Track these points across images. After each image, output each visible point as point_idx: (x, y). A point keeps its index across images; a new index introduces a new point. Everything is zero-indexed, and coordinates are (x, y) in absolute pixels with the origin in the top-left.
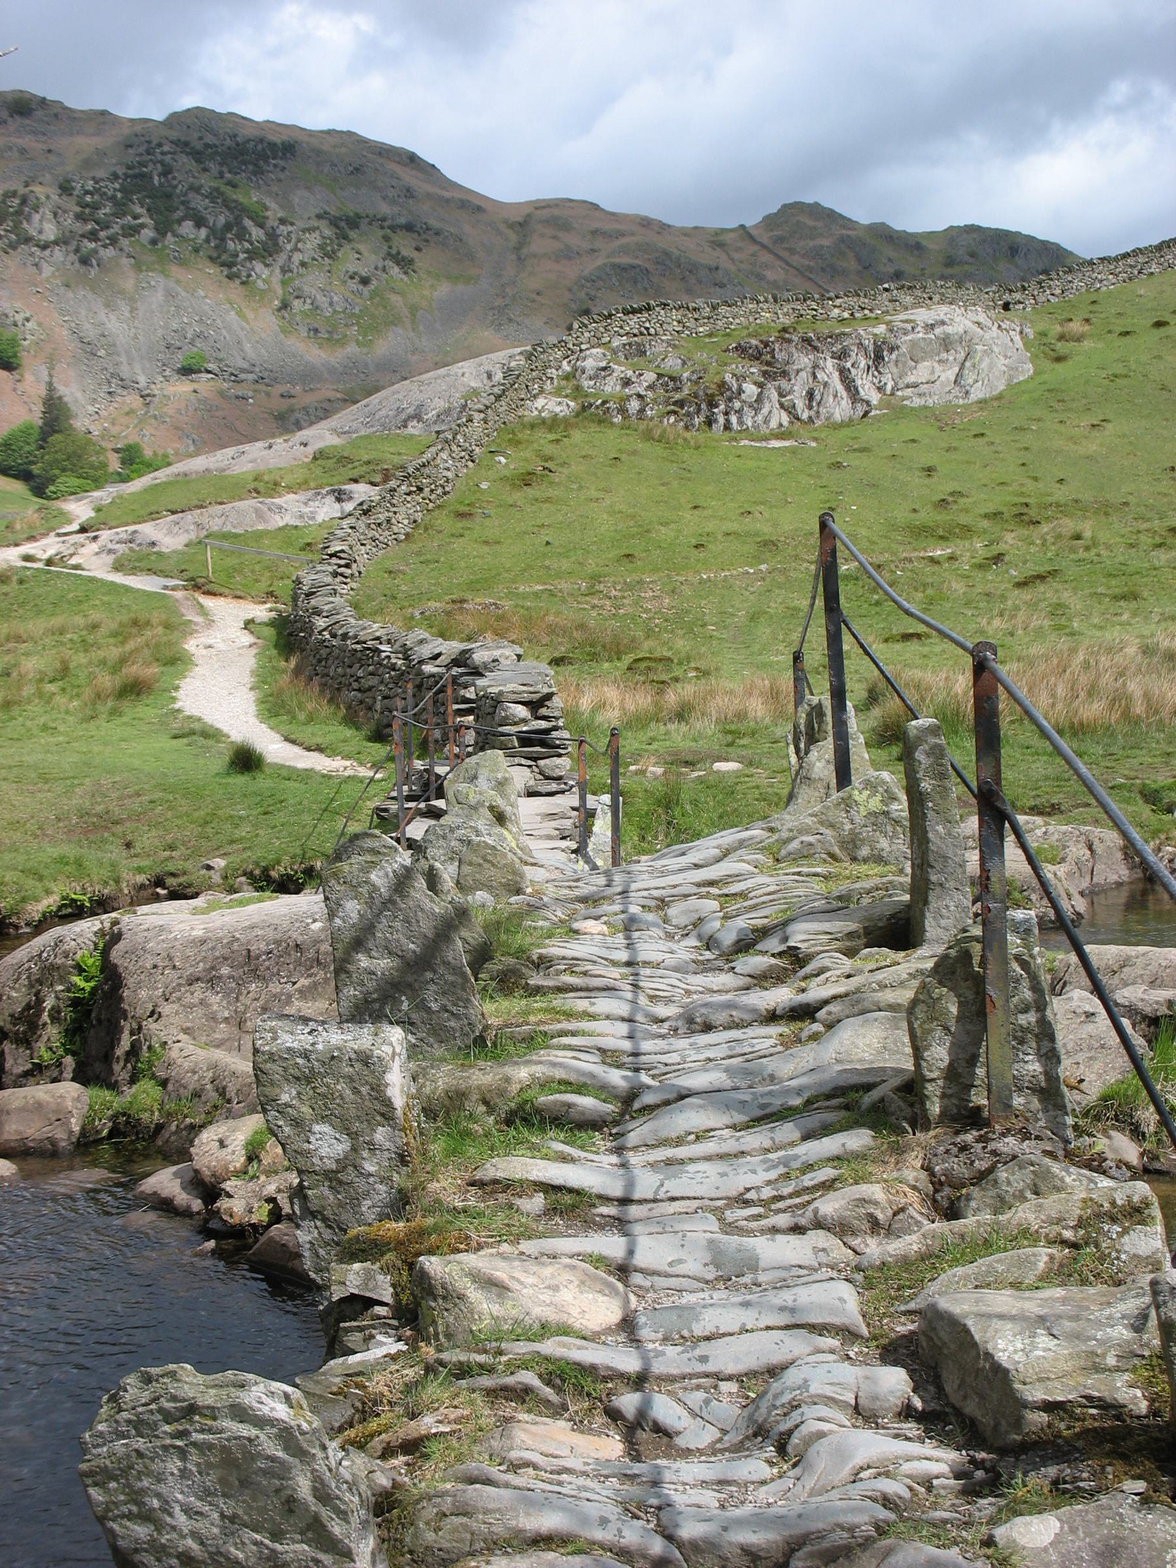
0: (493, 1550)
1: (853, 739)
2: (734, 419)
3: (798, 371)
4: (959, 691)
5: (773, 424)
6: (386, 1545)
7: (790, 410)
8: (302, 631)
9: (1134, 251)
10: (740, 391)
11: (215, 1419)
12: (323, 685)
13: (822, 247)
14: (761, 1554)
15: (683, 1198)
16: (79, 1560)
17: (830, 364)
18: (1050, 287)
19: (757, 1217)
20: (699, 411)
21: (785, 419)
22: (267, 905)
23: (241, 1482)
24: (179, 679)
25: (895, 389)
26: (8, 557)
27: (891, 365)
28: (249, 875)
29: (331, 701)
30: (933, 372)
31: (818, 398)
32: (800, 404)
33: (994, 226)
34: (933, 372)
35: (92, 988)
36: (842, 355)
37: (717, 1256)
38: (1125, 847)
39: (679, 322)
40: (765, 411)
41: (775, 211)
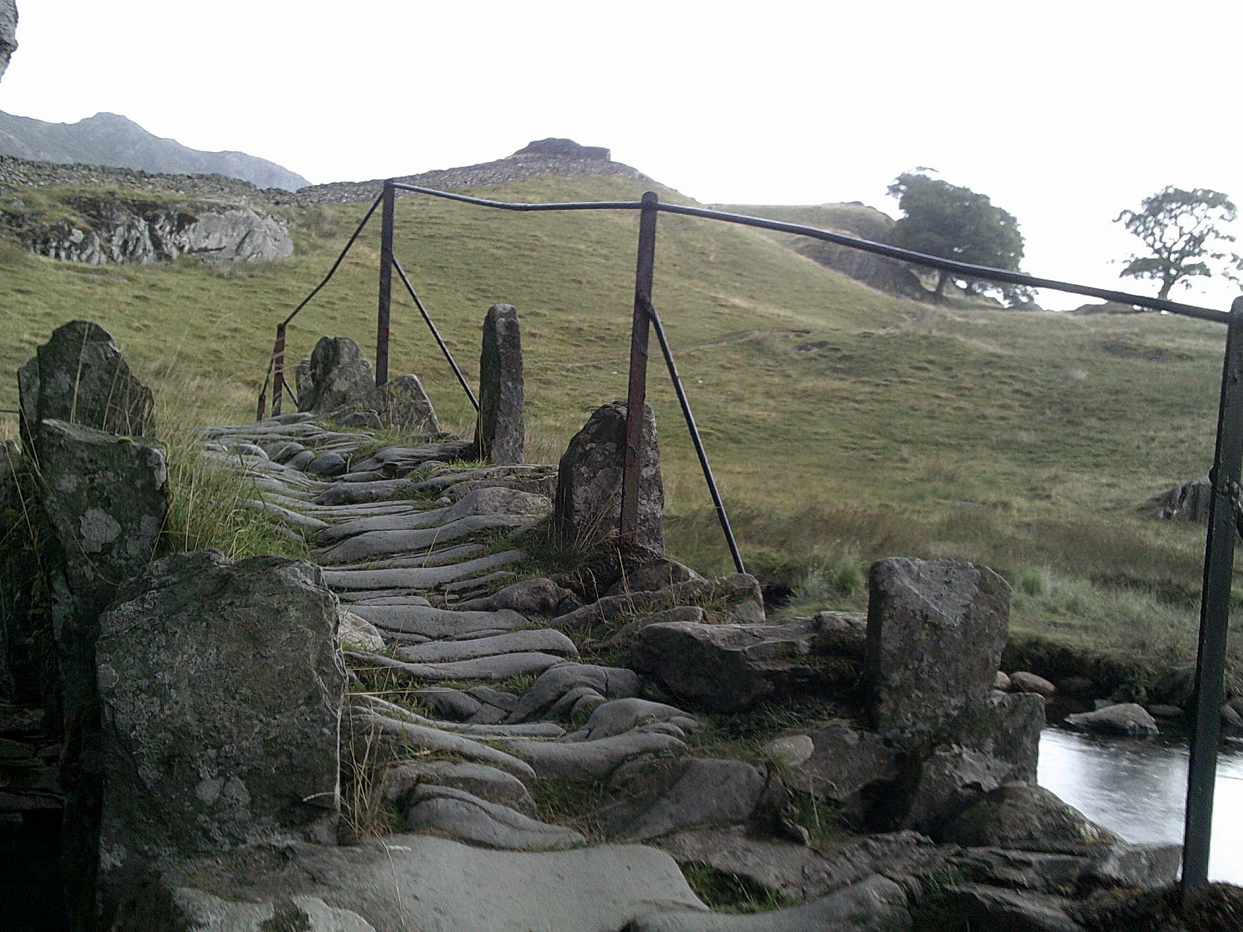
0: (422, 683)
2: (63, 254)
3: (118, 226)
4: (632, 218)
5: (95, 260)
6: (33, 546)
7: (111, 258)
10: (70, 233)
13: (928, 310)
16: (526, 651)
17: (142, 224)
19: (456, 601)
20: (961, 392)
21: (104, 258)
22: (1111, 708)
23: (600, 622)
25: (191, 251)
26: (969, 930)
27: (190, 233)
28: (1128, 735)
31: (131, 248)
32: (116, 251)
36: (152, 221)
38: (491, 678)
39: (25, 174)
40: (89, 251)
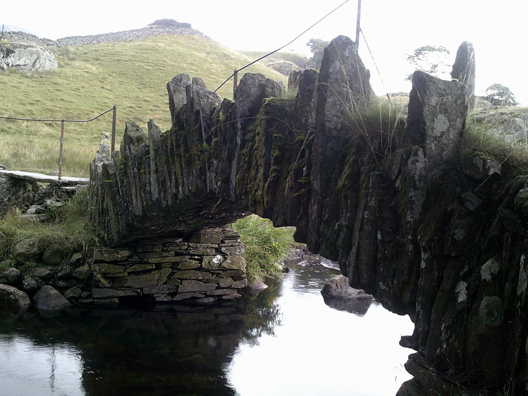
1: (118, 126)
8: (491, 307)
9: (65, 38)
11: (380, 124)
12: (68, 168)
14: (236, 89)
15: (358, 23)
18: (62, 42)
24: (229, 102)
29: (232, 359)
30: (25, 62)
33: (398, 390)
34: (25, 62)
35: (271, 168)
37: (71, 264)
41: (411, 88)
